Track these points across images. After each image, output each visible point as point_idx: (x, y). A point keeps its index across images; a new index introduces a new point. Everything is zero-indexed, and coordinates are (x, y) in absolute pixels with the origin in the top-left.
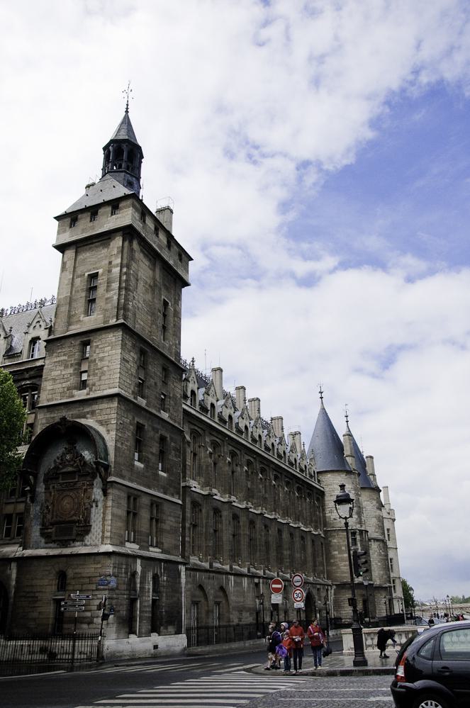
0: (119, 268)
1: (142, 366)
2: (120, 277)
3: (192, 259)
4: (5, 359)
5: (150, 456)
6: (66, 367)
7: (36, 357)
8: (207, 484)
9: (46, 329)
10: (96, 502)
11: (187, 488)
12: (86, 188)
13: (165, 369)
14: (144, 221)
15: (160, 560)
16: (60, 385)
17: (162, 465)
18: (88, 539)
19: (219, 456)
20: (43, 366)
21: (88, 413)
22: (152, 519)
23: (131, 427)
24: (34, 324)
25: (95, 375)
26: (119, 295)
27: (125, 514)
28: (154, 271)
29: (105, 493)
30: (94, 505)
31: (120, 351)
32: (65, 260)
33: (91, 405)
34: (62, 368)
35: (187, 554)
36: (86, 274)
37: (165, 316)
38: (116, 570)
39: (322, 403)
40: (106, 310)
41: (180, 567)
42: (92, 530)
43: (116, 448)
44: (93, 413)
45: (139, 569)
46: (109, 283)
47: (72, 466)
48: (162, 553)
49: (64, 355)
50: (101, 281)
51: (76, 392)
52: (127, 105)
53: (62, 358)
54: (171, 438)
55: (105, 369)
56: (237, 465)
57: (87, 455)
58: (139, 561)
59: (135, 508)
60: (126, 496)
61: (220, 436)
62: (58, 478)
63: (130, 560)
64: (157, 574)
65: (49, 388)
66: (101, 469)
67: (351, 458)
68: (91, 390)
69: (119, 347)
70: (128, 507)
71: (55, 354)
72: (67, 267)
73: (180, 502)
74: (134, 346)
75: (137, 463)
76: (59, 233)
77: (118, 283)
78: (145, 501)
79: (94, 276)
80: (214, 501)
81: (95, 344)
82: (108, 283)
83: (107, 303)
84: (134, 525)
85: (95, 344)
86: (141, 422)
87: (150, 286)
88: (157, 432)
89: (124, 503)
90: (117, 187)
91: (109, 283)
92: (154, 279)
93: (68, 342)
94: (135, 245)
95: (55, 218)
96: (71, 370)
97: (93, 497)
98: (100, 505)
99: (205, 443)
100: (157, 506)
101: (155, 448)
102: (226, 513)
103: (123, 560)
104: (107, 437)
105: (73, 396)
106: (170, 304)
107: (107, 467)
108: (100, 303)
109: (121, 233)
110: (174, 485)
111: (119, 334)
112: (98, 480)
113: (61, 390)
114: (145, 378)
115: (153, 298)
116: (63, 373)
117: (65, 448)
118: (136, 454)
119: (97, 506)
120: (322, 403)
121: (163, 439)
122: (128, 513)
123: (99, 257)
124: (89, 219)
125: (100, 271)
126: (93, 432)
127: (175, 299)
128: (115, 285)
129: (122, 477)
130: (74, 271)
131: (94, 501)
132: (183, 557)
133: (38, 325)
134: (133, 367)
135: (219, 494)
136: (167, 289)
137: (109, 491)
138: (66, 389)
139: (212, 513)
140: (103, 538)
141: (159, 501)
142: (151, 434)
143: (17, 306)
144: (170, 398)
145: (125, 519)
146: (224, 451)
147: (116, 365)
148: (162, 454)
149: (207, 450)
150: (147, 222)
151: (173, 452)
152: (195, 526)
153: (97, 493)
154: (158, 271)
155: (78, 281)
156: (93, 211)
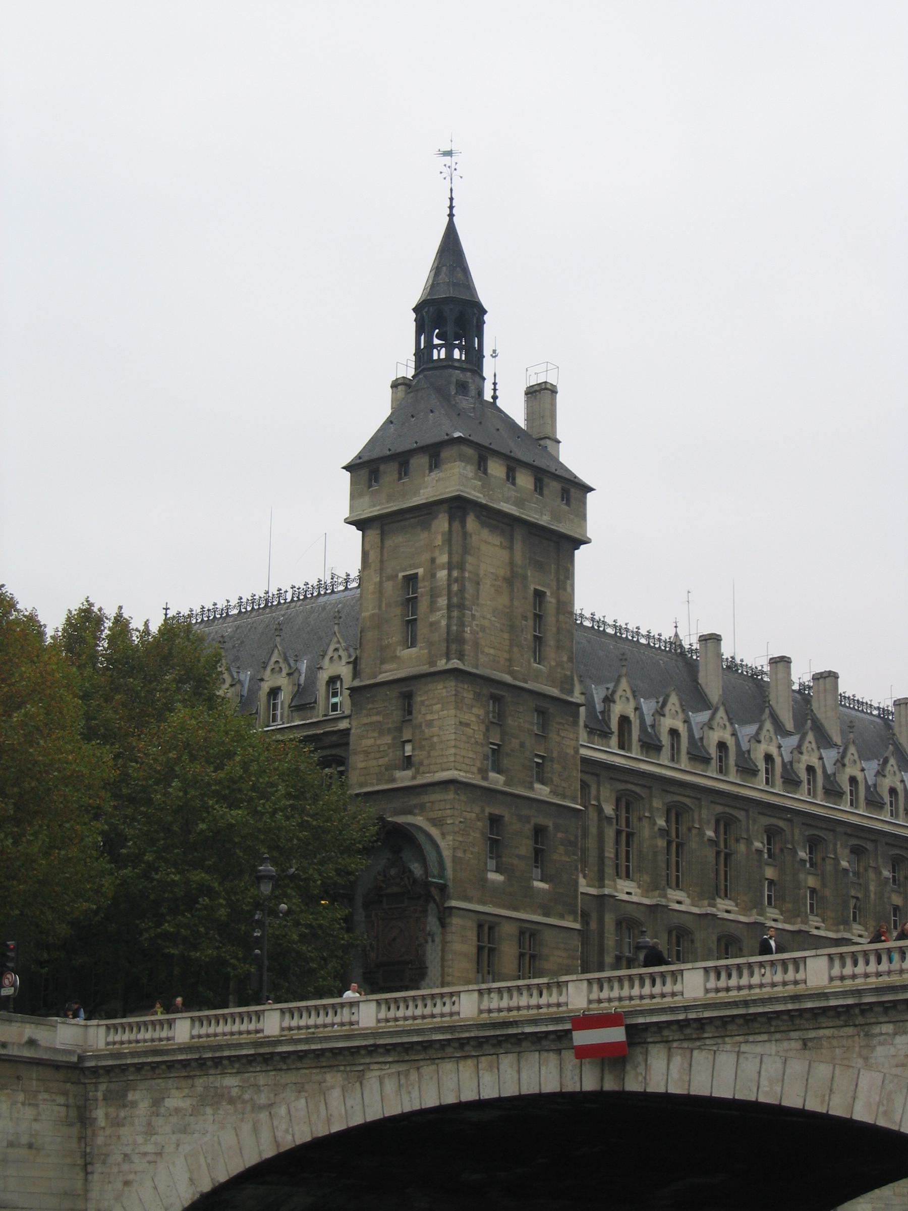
1: (498, 721)
2: (449, 586)
4: (292, 711)
5: (515, 861)
6: (381, 733)
8: (654, 887)
9: (348, 663)
10: (431, 935)
13: (542, 713)
14: (485, 472)
16: (374, 763)
21: (415, 806)
22: (522, 955)
23: (479, 824)
24: (330, 653)
25: (422, 748)
26: (449, 617)
28: (511, 548)
29: (443, 924)
30: (430, 939)
32: (367, 547)
34: (375, 734)
36: (401, 575)
37: (538, 618)
42: (429, 973)
43: (455, 859)
44: (422, 807)
49: (378, 714)
50: (423, 588)
51: (398, 774)
52: (451, 199)
53: (375, 718)
54: (557, 827)
55: (435, 739)
56: (737, 841)
57: (416, 869)
65: (361, 765)
68: (417, 772)
71: (364, 712)
72: (370, 561)
73: (577, 926)
74: (478, 696)
76: (353, 497)
77: (446, 598)
78: (509, 929)
79: (411, 580)
80: (671, 912)
82: (432, 596)
86: (497, 812)
87: (505, 579)
88: (529, 822)
91: (433, 595)
92: (512, 563)
94: (471, 523)
95: (343, 468)
96: (388, 739)
97: (428, 928)
98: (438, 939)
99: (651, 809)
101: (525, 847)
104: (442, 844)
105: (393, 780)
106: (548, 594)
108: (422, 630)
109: (445, 507)
110: (564, 899)
112: (432, 906)
114: (502, 740)
115: (512, 600)
116: (378, 742)
117: (388, 859)
119: (433, 941)
121: (539, 832)
122: (480, 949)
124: (396, 476)
125: (421, 571)
126: (422, 839)
127: (558, 580)
128: (442, 602)
129: (466, 898)
130: (382, 569)
131: (429, 934)
133: (336, 656)
135: (687, 901)
136: (540, 566)
138: (383, 768)
143: (303, 587)
144: (552, 760)
145: (475, 957)
146: (700, 820)
148: (539, 856)
149: (655, 824)
150: (489, 471)
153: (432, 923)
154: (518, 546)
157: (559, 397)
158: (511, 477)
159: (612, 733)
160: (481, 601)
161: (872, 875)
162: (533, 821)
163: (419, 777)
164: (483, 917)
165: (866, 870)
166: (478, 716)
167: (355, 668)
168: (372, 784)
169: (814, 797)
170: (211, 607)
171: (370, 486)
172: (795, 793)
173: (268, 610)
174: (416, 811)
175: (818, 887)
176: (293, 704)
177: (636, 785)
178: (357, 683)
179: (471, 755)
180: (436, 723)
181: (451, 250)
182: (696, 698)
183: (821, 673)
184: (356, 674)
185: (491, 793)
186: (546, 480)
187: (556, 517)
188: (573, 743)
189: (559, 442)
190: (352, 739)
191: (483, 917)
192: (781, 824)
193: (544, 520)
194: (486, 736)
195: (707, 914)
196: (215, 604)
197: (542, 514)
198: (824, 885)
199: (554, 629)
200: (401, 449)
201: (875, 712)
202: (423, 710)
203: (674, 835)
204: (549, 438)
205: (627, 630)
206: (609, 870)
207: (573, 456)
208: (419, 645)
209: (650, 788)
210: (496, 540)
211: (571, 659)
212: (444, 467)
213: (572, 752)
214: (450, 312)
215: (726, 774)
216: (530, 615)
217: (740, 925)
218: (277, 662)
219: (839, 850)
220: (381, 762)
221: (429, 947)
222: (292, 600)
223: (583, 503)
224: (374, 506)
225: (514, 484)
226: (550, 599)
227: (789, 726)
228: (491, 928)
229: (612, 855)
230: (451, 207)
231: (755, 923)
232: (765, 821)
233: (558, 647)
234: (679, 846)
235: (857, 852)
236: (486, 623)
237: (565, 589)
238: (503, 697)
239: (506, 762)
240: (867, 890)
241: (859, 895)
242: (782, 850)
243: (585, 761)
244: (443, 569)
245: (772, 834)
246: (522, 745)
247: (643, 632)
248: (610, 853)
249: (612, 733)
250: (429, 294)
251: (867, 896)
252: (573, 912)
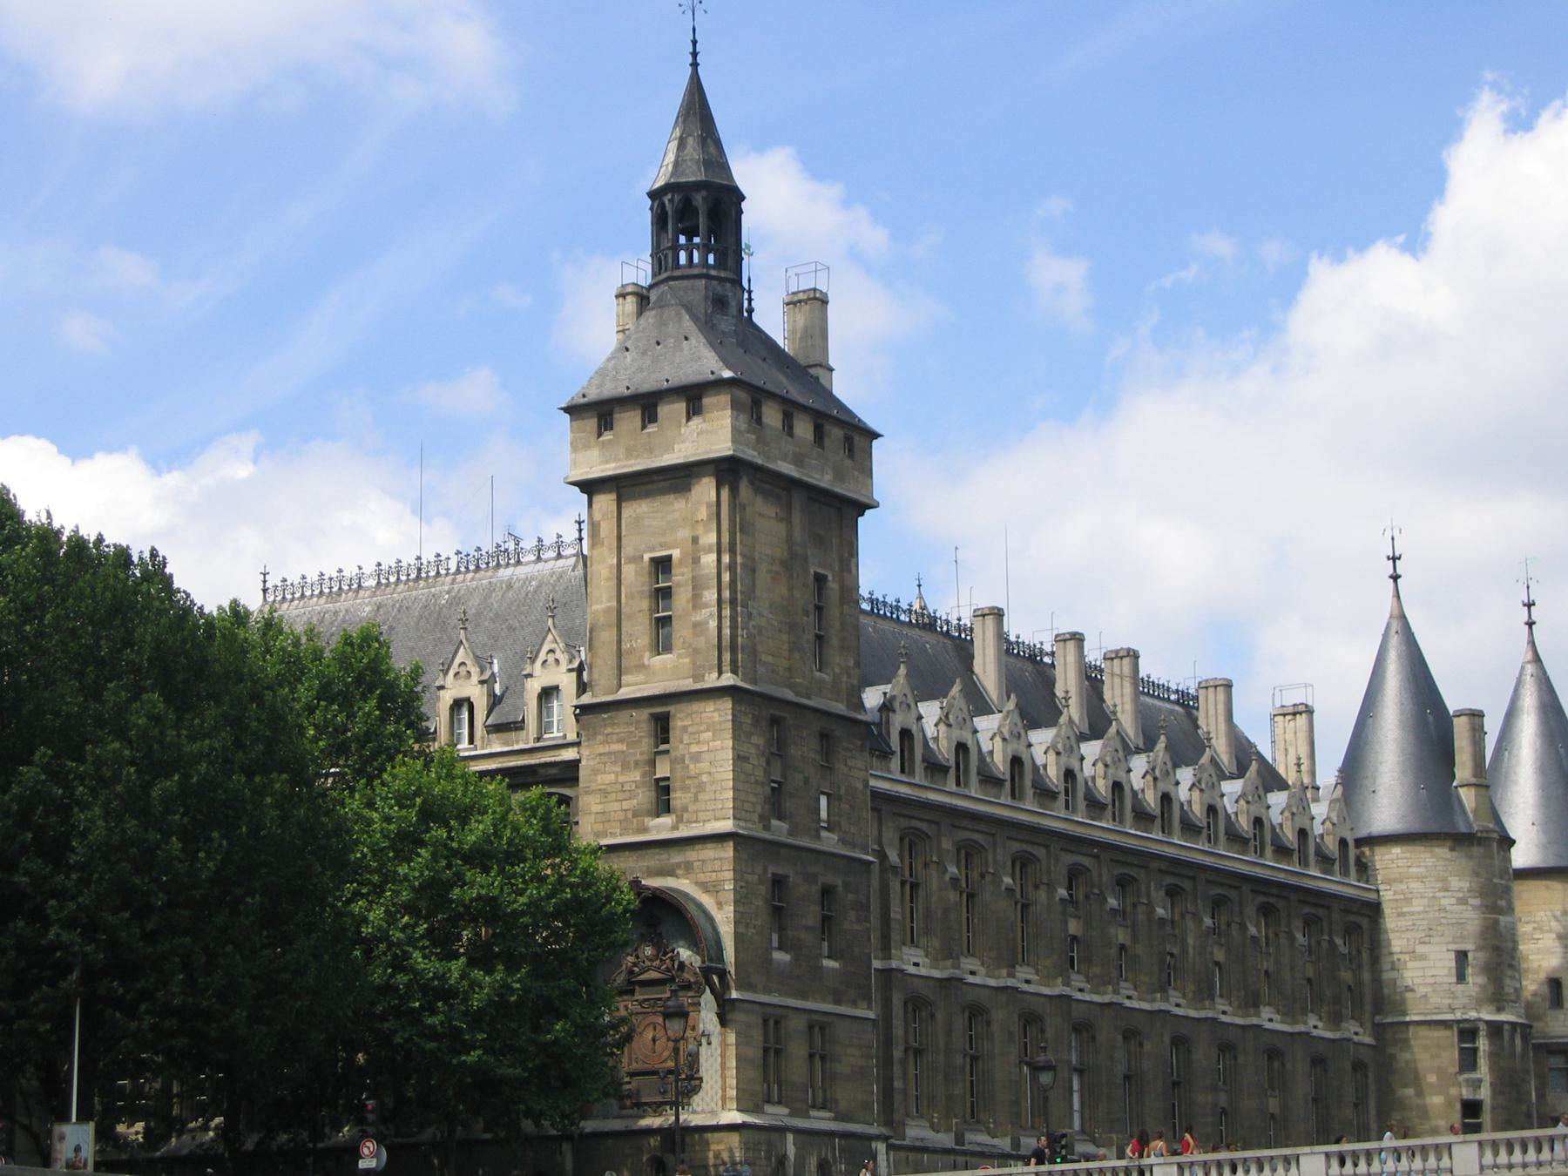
0: (714, 556)
1: (778, 751)
3: (877, 436)
5: (803, 935)
6: (626, 767)
7: (554, 735)
8: (948, 953)
9: (570, 670)
11: (888, 976)
12: (617, 297)
14: (759, 420)
15: (831, 1134)
16: (617, 806)
17: (830, 947)
18: (697, 1101)
19: (982, 876)
20: (579, 761)
21: (678, 865)
22: (811, 1056)
24: (542, 656)
26: (720, 617)
27: (760, 1054)
28: (788, 520)
29: (723, 1021)
30: (704, 1041)
31: (730, 743)
33: (666, 704)
34: (618, 769)
35: (897, 1117)
36: (647, 557)
38: (751, 1154)
39: (1397, 596)
40: (696, 651)
41: (874, 1145)
43: (738, 937)
44: (688, 867)
45: (791, 1150)
46: (697, 587)
47: (657, 969)
48: (835, 1119)
49: (620, 741)
50: (680, 577)
52: (694, 42)
53: (616, 747)
54: (846, 885)
56: (1037, 887)
58: (790, 1137)
59: (778, 1041)
60: (760, 1021)
61: (982, 827)
62: (632, 992)
63: (774, 1136)
64: (826, 1159)
66: (713, 972)
67: (1473, 791)
68: (680, 820)
69: (729, 734)
70: (766, 1041)
71: (600, 738)
74: (757, 720)
75: (778, 956)
81: (680, 724)
82: (694, 588)
83: (696, 635)
84: (778, 1072)
85: (680, 724)
86: (781, 871)
89: (757, 1035)
90: (693, 341)
91: (697, 587)
92: (790, 540)
93: (623, 715)
94: (745, 489)
96: (636, 776)
98: (715, 1041)
100: (822, 1029)
102: (1001, 1016)
103: (762, 1136)
105: (645, 830)
107: (723, 974)
108: (680, 632)
109: (712, 467)
110: (854, 985)
111: (727, 705)
113: (621, 815)
114: (784, 776)
115: (791, 589)
116: (622, 779)
118: (775, 937)
120: (1397, 596)
122: (766, 1050)
123: (670, 518)
125: (676, 554)
126: (692, 909)
127: (841, 559)
128: (711, 596)
130: (619, 547)
132: (888, 1122)
134: (757, 766)
135: (982, 970)
136: (819, 541)
137: (729, 1017)
138: (630, 815)
139: (960, 1022)
140: (724, 1099)
141: (825, 1019)
142: (803, 891)
146: (995, 861)
147: (725, 771)
149: (946, 870)
150: (764, 420)
151: (852, 913)
152: (918, 1052)
154: (797, 518)
155: (629, 571)
156: (647, 404)
157: (831, 309)
159: (893, 753)
160: (758, 593)
161: (1190, 924)
162: (821, 880)
163: (681, 826)
164: (770, 1010)
165: (1183, 917)
166: (758, 746)
167: (580, 677)
168: (613, 835)
169: (1121, 822)
170: (335, 575)
171: (600, 435)
172: (1099, 818)
173: (422, 583)
174: (680, 872)
175: (1128, 943)
176: (489, 722)
177: (921, 820)
178: (587, 699)
179: (752, 798)
180: (706, 757)
181: (697, 112)
183: (1117, 652)
184: (582, 688)
185: (773, 848)
186: (827, 427)
187: (840, 476)
188: (862, 774)
189: (832, 370)
190: (582, 773)
191: (770, 1010)
192: (1086, 861)
193: (825, 480)
194: (767, 772)
195: (1006, 988)
196: (340, 571)
197: (823, 472)
198: (1135, 939)
199: (838, 625)
200: (646, 387)
201: (1173, 697)
202: (686, 739)
203: (907, 873)
204: (821, 365)
205: (885, 603)
206: (895, 937)
207: (850, 387)
208: (676, 651)
209: (937, 823)
210: (771, 510)
211: (858, 664)
212: (708, 416)
213: (860, 786)
215: (1021, 798)
216: (811, 608)
217: (1042, 999)
218: (463, 664)
219: (1153, 893)
220: (626, 805)
221: (704, 1050)
222: (458, 571)
223: (868, 453)
224: (607, 462)
225: (791, 434)
226: (833, 585)
228: (777, 1023)
229: (899, 917)
230: (695, 54)
231: (1060, 996)
232: (1069, 859)
233: (843, 648)
234: (914, 886)
235: (1173, 893)
236: (763, 622)
237: (849, 571)
238: (783, 719)
239: (788, 805)
240: (1184, 942)
241: (1175, 951)
242: (1087, 897)
243: (877, 795)
244: (710, 551)
245: (1074, 875)
246: (806, 781)
248: (896, 913)
249: (893, 753)
250: (672, 174)
251: (1184, 951)
252: (867, 997)
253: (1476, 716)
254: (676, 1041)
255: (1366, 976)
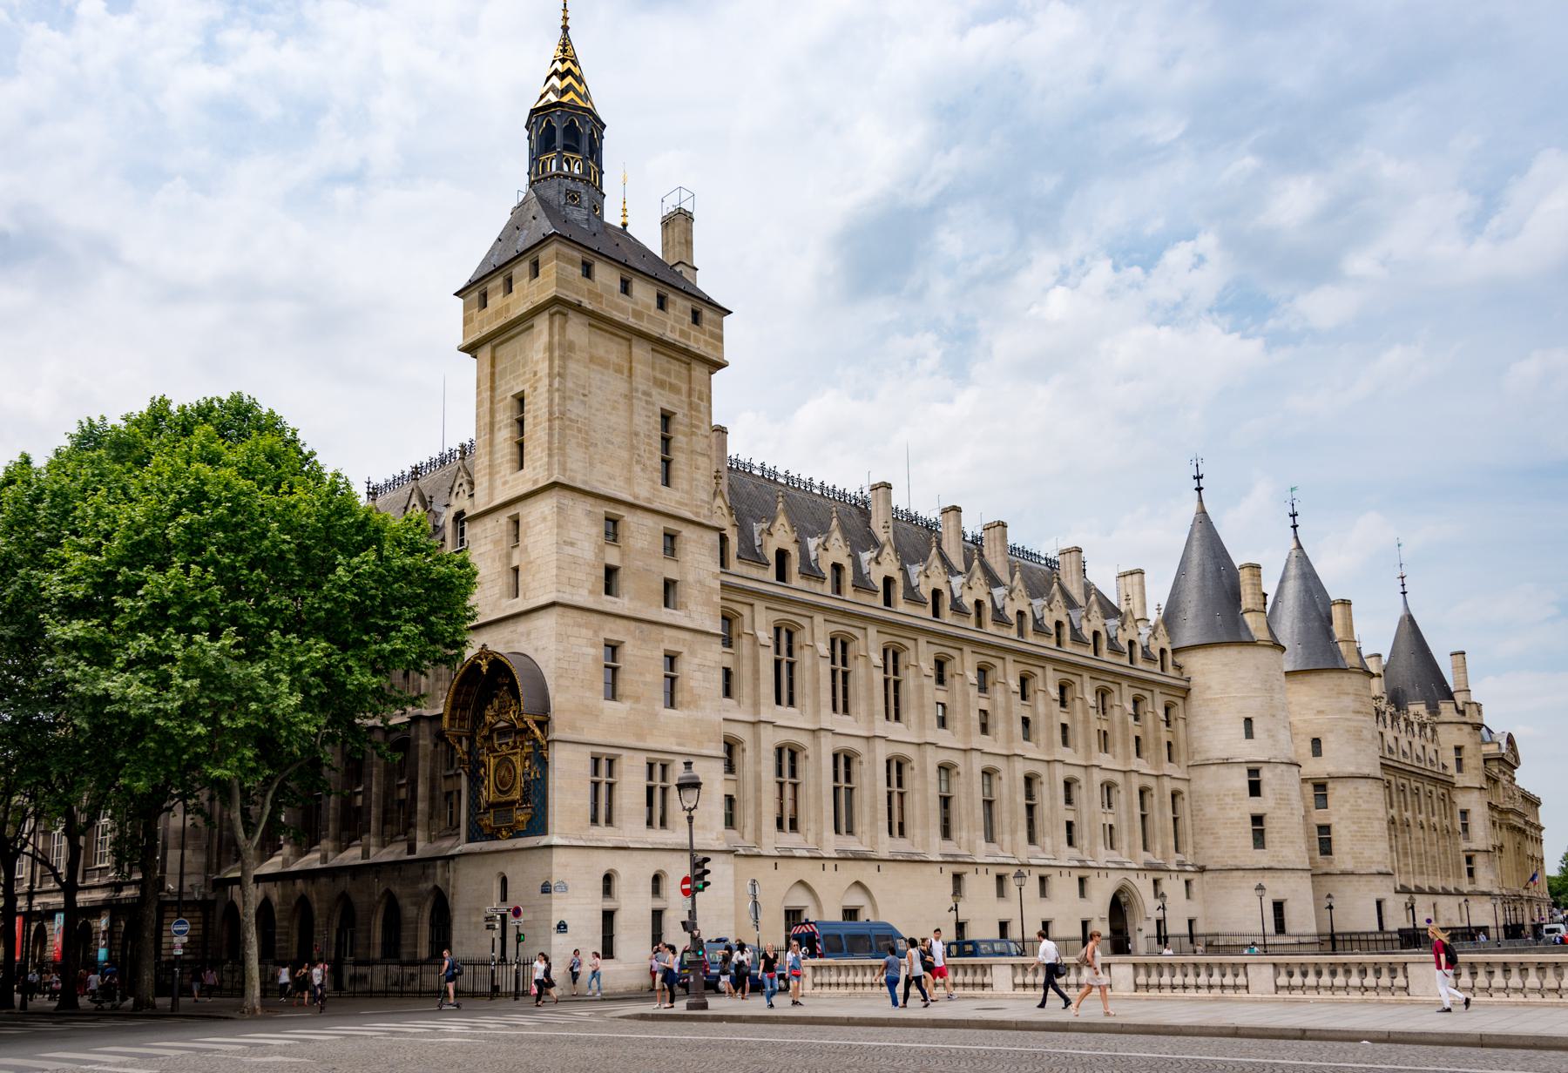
24: (456, 489)
39: (1201, 500)
120: (1201, 500)
158: (625, 288)
181: (567, 66)
182: (861, 537)
205: (799, 480)
214: (565, 132)
227: (961, 567)
228: (611, 762)
247: (817, 483)
253: (1255, 568)
254: (690, 810)
255: (556, 338)
